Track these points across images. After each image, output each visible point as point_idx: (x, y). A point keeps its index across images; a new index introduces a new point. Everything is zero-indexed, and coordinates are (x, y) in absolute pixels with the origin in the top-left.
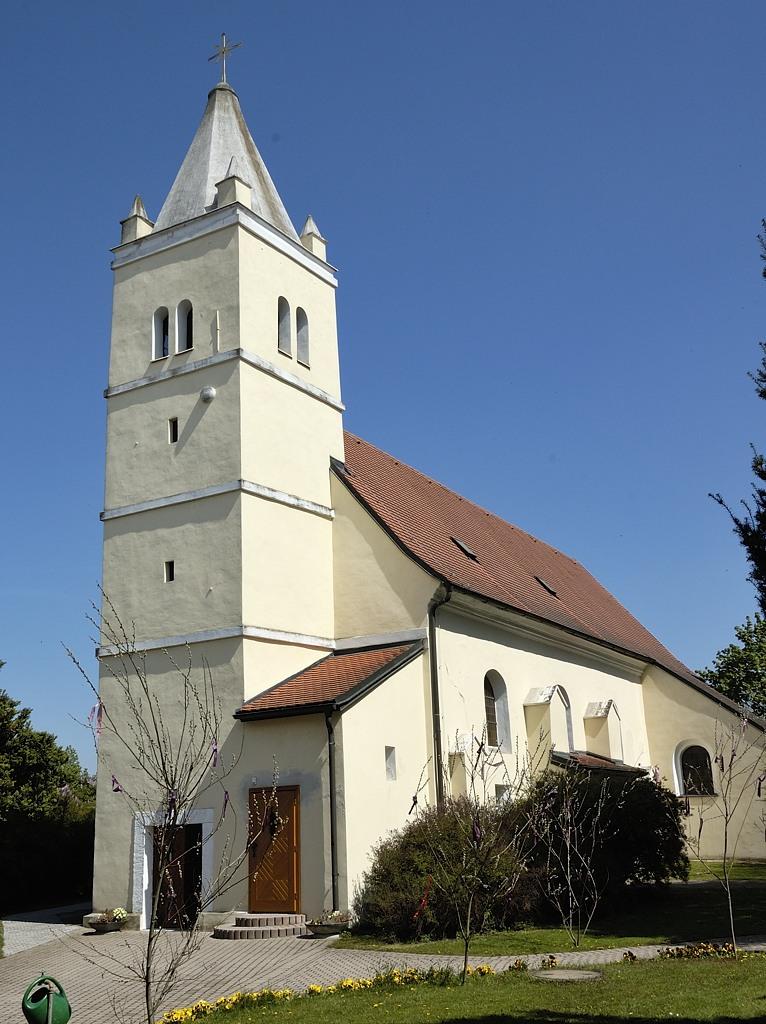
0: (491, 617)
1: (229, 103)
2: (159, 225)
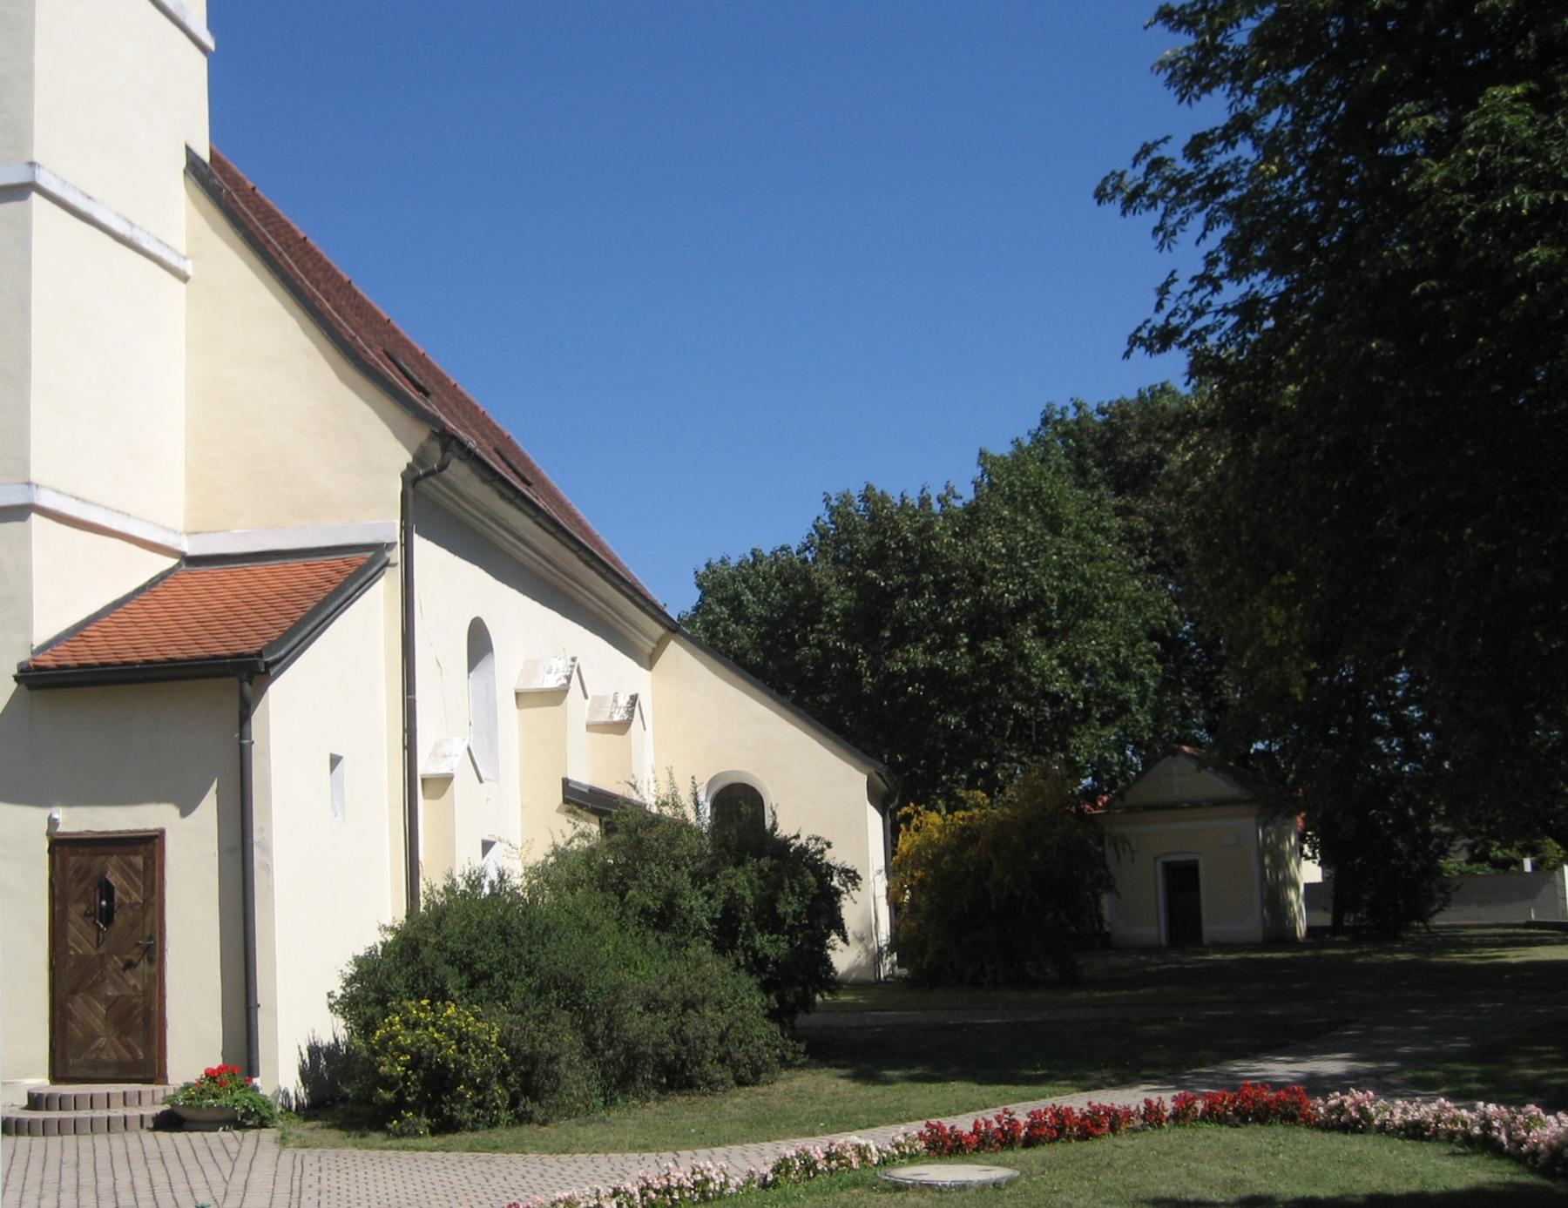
0: (486, 514)
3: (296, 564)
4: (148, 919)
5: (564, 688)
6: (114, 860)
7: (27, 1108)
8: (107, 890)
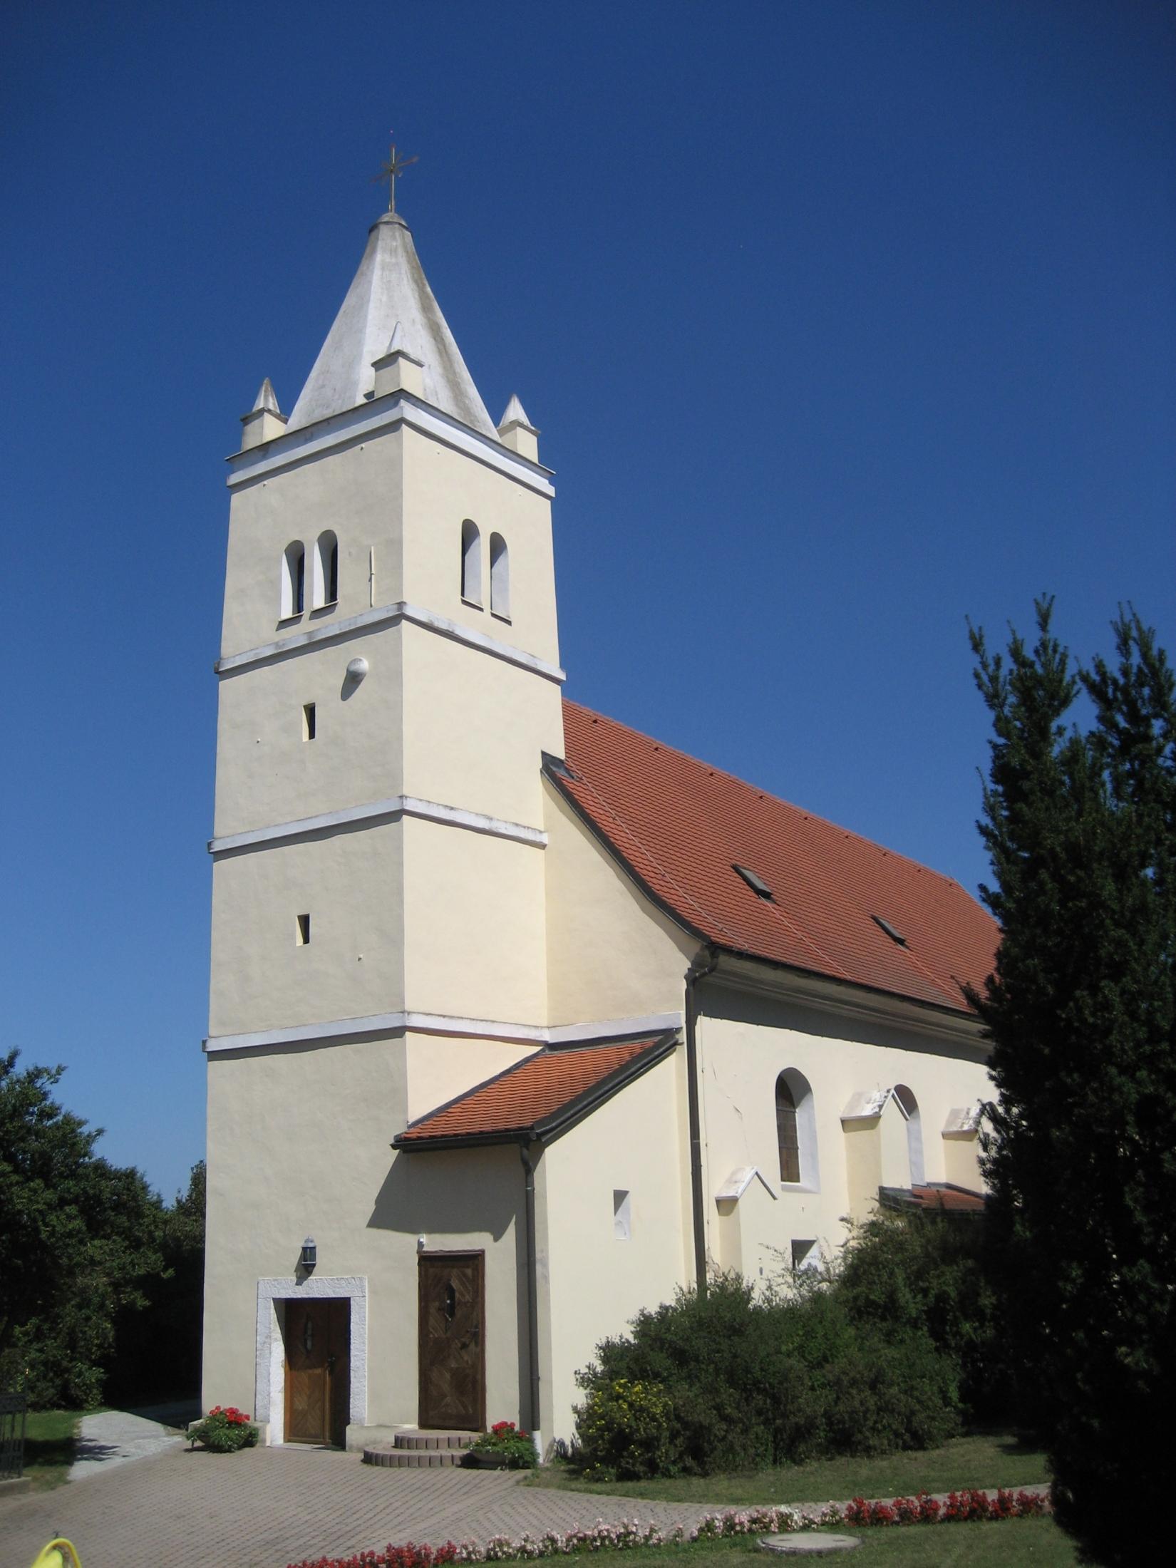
1: (397, 243)
2: (298, 419)
3: (612, 1047)
4: (475, 1313)
5: (877, 1115)
6: (455, 1272)
7: (396, 1447)
8: (451, 1292)
